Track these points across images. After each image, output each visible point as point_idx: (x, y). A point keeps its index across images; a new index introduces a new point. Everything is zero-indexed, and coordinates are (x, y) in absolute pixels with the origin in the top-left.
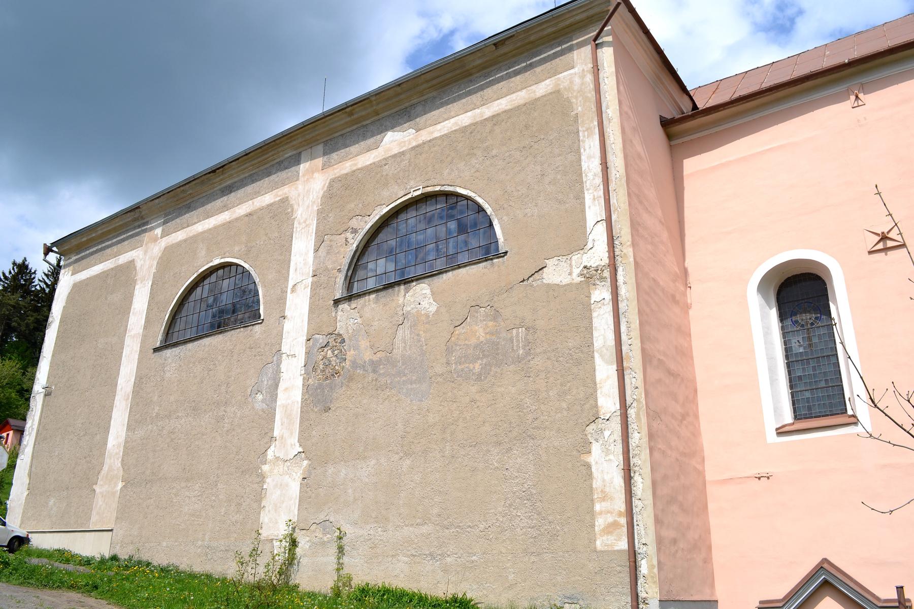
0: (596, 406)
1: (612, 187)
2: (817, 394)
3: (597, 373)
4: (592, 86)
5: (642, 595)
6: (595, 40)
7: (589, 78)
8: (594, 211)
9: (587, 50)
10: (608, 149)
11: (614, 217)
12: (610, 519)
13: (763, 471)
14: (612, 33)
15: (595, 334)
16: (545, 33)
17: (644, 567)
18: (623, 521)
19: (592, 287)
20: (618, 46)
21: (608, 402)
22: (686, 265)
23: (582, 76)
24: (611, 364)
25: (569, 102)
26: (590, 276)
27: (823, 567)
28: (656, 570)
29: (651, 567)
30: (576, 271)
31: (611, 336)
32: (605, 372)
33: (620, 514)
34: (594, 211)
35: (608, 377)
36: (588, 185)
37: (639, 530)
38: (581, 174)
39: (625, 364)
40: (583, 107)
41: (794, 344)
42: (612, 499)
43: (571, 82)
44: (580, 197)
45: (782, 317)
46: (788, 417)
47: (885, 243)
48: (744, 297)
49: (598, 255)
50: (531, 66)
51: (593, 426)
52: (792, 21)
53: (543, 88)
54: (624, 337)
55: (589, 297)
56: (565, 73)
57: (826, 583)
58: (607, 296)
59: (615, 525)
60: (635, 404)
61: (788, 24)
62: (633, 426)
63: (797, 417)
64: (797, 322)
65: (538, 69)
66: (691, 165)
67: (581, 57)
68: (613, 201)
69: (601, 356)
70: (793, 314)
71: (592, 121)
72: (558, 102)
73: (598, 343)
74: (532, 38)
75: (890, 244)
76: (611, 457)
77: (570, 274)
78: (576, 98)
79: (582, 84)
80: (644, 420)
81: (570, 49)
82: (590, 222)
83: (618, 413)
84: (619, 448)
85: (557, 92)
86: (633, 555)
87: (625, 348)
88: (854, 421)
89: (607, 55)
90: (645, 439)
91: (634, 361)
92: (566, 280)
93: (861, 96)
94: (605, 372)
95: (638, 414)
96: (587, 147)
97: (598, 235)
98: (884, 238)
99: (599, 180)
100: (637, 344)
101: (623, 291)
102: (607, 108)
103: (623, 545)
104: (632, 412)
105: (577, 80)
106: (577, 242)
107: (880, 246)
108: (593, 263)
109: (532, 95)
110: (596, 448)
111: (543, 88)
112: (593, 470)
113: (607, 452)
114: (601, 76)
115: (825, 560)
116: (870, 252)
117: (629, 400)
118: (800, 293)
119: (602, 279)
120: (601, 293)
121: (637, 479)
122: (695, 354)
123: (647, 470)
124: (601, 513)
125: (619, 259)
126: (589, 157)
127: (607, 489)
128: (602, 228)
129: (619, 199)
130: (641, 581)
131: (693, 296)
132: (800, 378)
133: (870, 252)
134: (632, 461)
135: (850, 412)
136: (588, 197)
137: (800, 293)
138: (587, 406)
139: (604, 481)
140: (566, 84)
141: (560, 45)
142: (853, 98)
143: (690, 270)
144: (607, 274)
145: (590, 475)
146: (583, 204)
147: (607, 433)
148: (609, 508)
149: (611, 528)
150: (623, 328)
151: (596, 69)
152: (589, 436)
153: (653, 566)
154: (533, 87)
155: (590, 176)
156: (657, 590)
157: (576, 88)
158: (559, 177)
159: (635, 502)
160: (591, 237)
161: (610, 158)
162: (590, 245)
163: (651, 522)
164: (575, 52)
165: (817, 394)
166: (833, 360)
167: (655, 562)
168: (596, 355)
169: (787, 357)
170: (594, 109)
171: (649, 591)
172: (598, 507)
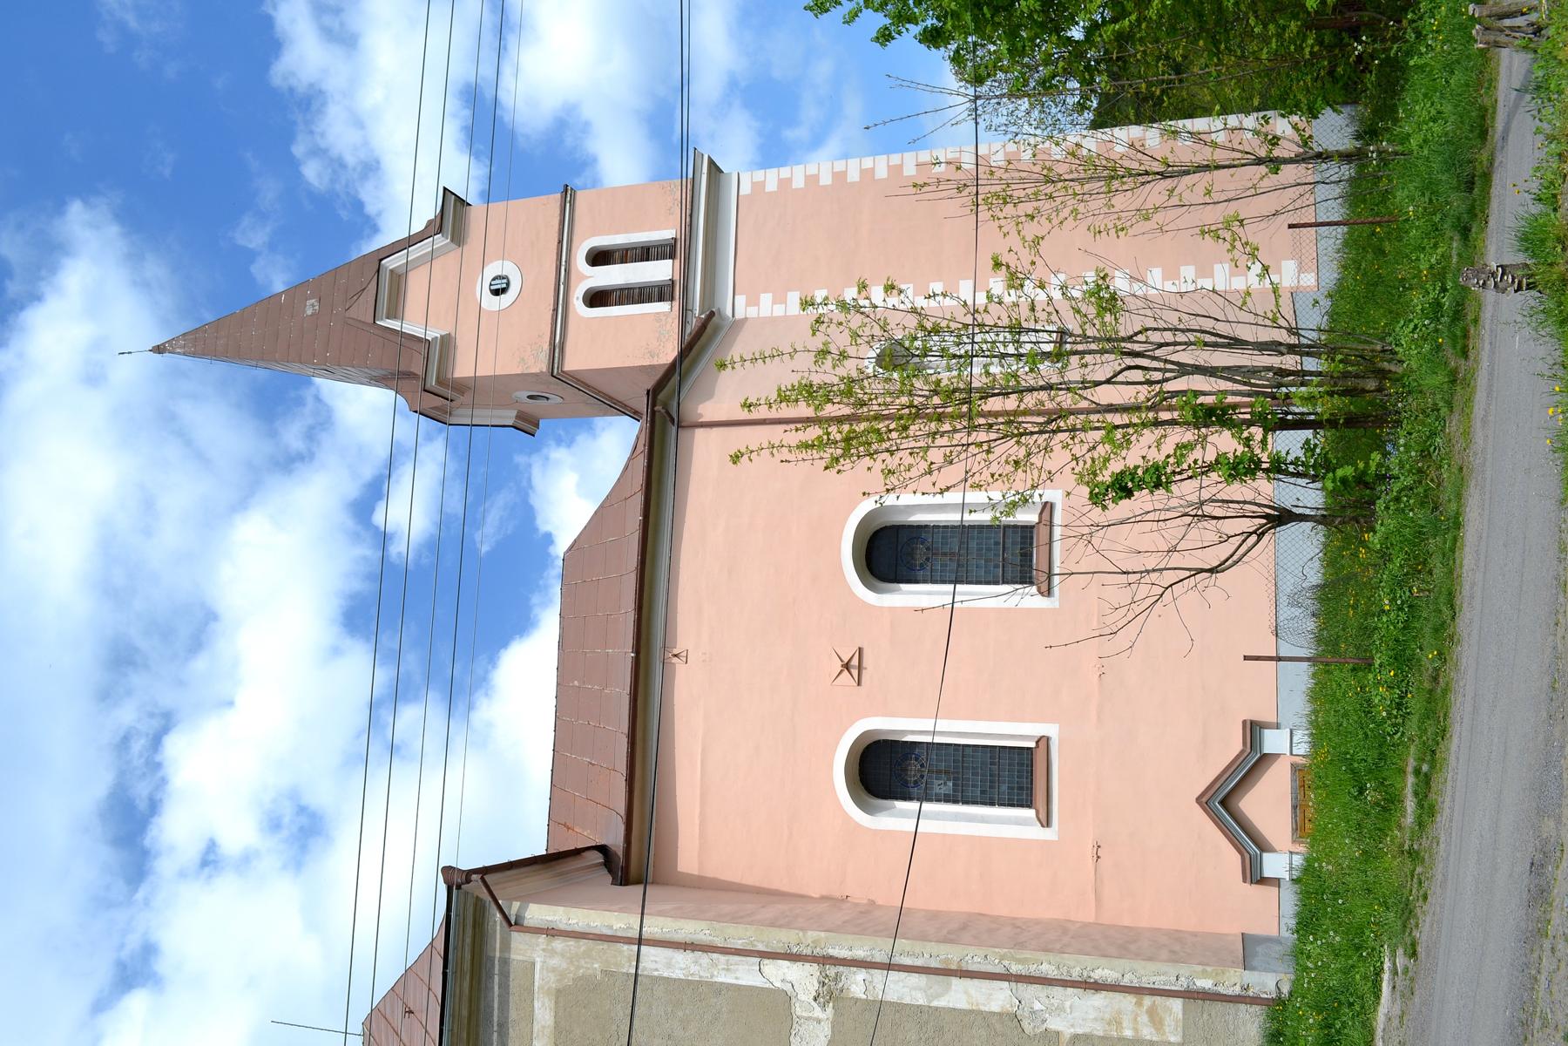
0: (1000, 1014)
1: (719, 942)
2: (1007, 776)
3: (958, 1006)
4: (572, 942)
5: (1237, 990)
6: (510, 925)
7: (558, 944)
8: (745, 974)
9: (518, 940)
10: (668, 937)
11: (761, 947)
12: (1144, 1018)
13: (1089, 851)
14: (511, 900)
15: (907, 1000)
16: (466, 991)
17: (1205, 984)
18: (1148, 1001)
19: (844, 994)
20: (527, 898)
21: (997, 998)
22: (815, 893)
23: (553, 953)
24: (949, 985)
25: (581, 978)
26: (829, 994)
27: (1204, 801)
28: (1209, 969)
29: (1205, 974)
30: (818, 1012)
31: (914, 979)
32: (959, 995)
33: (1139, 1004)
34: (745, 974)
35: (966, 992)
36: (705, 975)
37: (1160, 982)
38: (689, 982)
39: (954, 967)
40: (595, 961)
41: (943, 790)
42: (1119, 1012)
43: (554, 970)
44: (720, 989)
45: (906, 797)
46: (1029, 813)
47: (853, 666)
48: (876, 832)
49: (801, 979)
50: (503, 1026)
51: (1025, 1024)
52: (302, 810)
53: (543, 1013)
54: (919, 962)
55: (857, 1000)
56: (537, 976)
57: (1223, 803)
58: (861, 975)
59: (1152, 1013)
60: (1006, 963)
61: (304, 820)
62: (1032, 970)
63: (1028, 804)
64: (916, 782)
65: (513, 1015)
66: (688, 860)
67: (523, 948)
68: (739, 944)
69: (938, 996)
70: (905, 784)
71: (621, 952)
72: (570, 997)
73: (921, 1000)
74: (465, 1013)
75: (855, 662)
76: (1068, 1004)
77: (819, 1021)
78: (578, 968)
79: (563, 955)
80: (1027, 954)
81: (505, 962)
82: (757, 981)
83: (1013, 984)
84: (1058, 991)
85: (559, 994)
86: (1189, 995)
87: (934, 964)
88: (1044, 741)
89: (537, 913)
90: (1051, 957)
91: (951, 954)
92: (826, 1029)
93: (676, 651)
94: (959, 995)
95: (1019, 961)
96: (654, 966)
97: (779, 974)
98: (847, 666)
99: (705, 958)
100: (932, 948)
101: (860, 953)
102: (611, 927)
103: (1177, 1005)
104: (1015, 969)
105: (555, 962)
106: (779, 1003)
107: (855, 672)
108: (813, 986)
109: (547, 1031)
110: (1054, 1024)
111: (543, 1013)
112: (1080, 1031)
113: (1060, 1009)
114: (562, 927)
115: (1198, 800)
116: (859, 684)
117: (999, 970)
118: (884, 770)
119: (837, 978)
120: (857, 984)
121: (1098, 975)
122: (934, 908)
123: (1089, 961)
124: (1136, 1030)
125: (817, 951)
126: (669, 965)
127: (1107, 1016)
128: (770, 967)
129: (739, 936)
130: (1221, 989)
131: (859, 895)
132: (983, 792)
133: (859, 684)
134: (1075, 976)
135: (1032, 745)
136: (722, 978)
137: (884, 770)
138: (998, 1026)
139: (1096, 1019)
140: (552, 977)
141: (492, 977)
142: (675, 660)
143: (824, 893)
144: (832, 971)
145: (1087, 1037)
146: (729, 987)
147: (1037, 1006)
148: (1130, 1017)
149: (1155, 1018)
150: (908, 961)
151: (551, 932)
152: (1038, 1031)
153: (1204, 971)
154: (536, 1028)
155: (694, 969)
156: (1232, 971)
157: (564, 965)
158: (680, 1014)
159: (1126, 981)
160: (778, 984)
161: (680, 937)
162: (787, 987)
163: (1152, 966)
164: (513, 956)
165: (1007, 776)
166: (968, 751)
167: (1200, 968)
168: (935, 1004)
169: (955, 802)
170: (606, 945)
171: (1233, 981)
172: (1128, 1033)
